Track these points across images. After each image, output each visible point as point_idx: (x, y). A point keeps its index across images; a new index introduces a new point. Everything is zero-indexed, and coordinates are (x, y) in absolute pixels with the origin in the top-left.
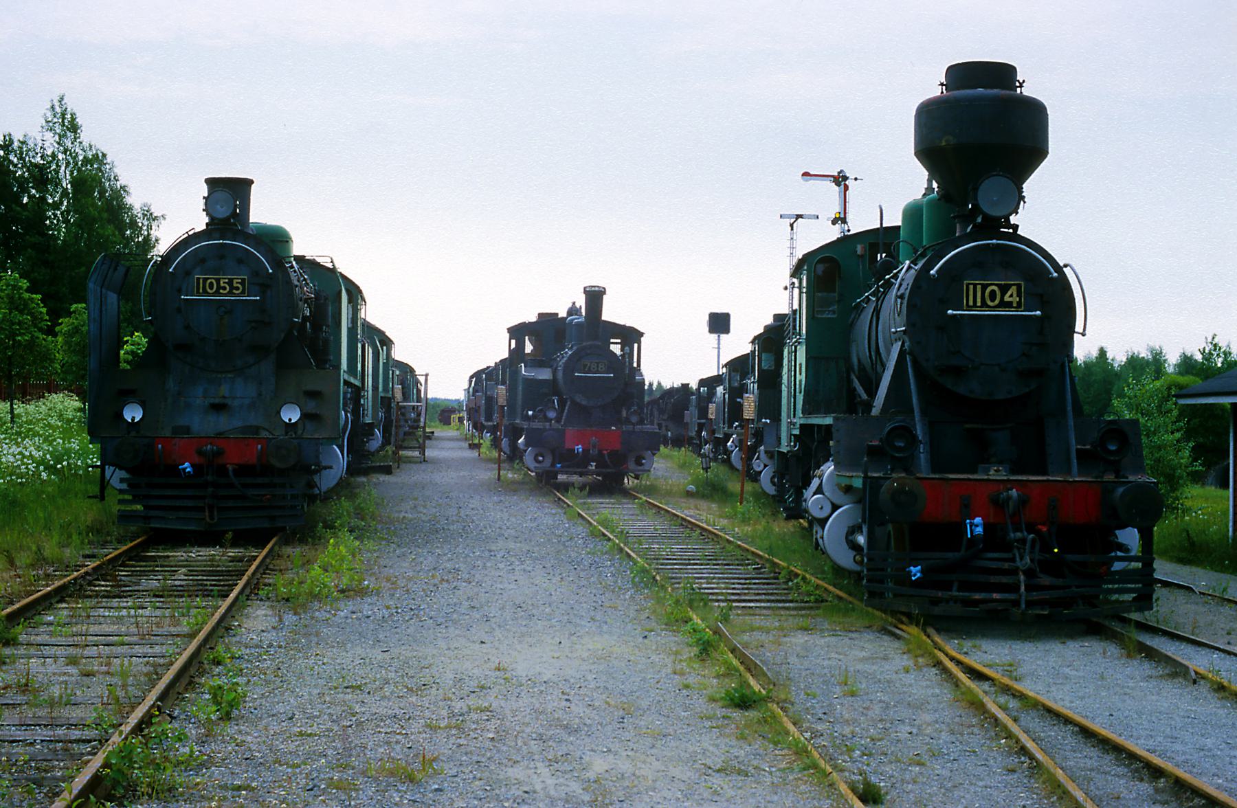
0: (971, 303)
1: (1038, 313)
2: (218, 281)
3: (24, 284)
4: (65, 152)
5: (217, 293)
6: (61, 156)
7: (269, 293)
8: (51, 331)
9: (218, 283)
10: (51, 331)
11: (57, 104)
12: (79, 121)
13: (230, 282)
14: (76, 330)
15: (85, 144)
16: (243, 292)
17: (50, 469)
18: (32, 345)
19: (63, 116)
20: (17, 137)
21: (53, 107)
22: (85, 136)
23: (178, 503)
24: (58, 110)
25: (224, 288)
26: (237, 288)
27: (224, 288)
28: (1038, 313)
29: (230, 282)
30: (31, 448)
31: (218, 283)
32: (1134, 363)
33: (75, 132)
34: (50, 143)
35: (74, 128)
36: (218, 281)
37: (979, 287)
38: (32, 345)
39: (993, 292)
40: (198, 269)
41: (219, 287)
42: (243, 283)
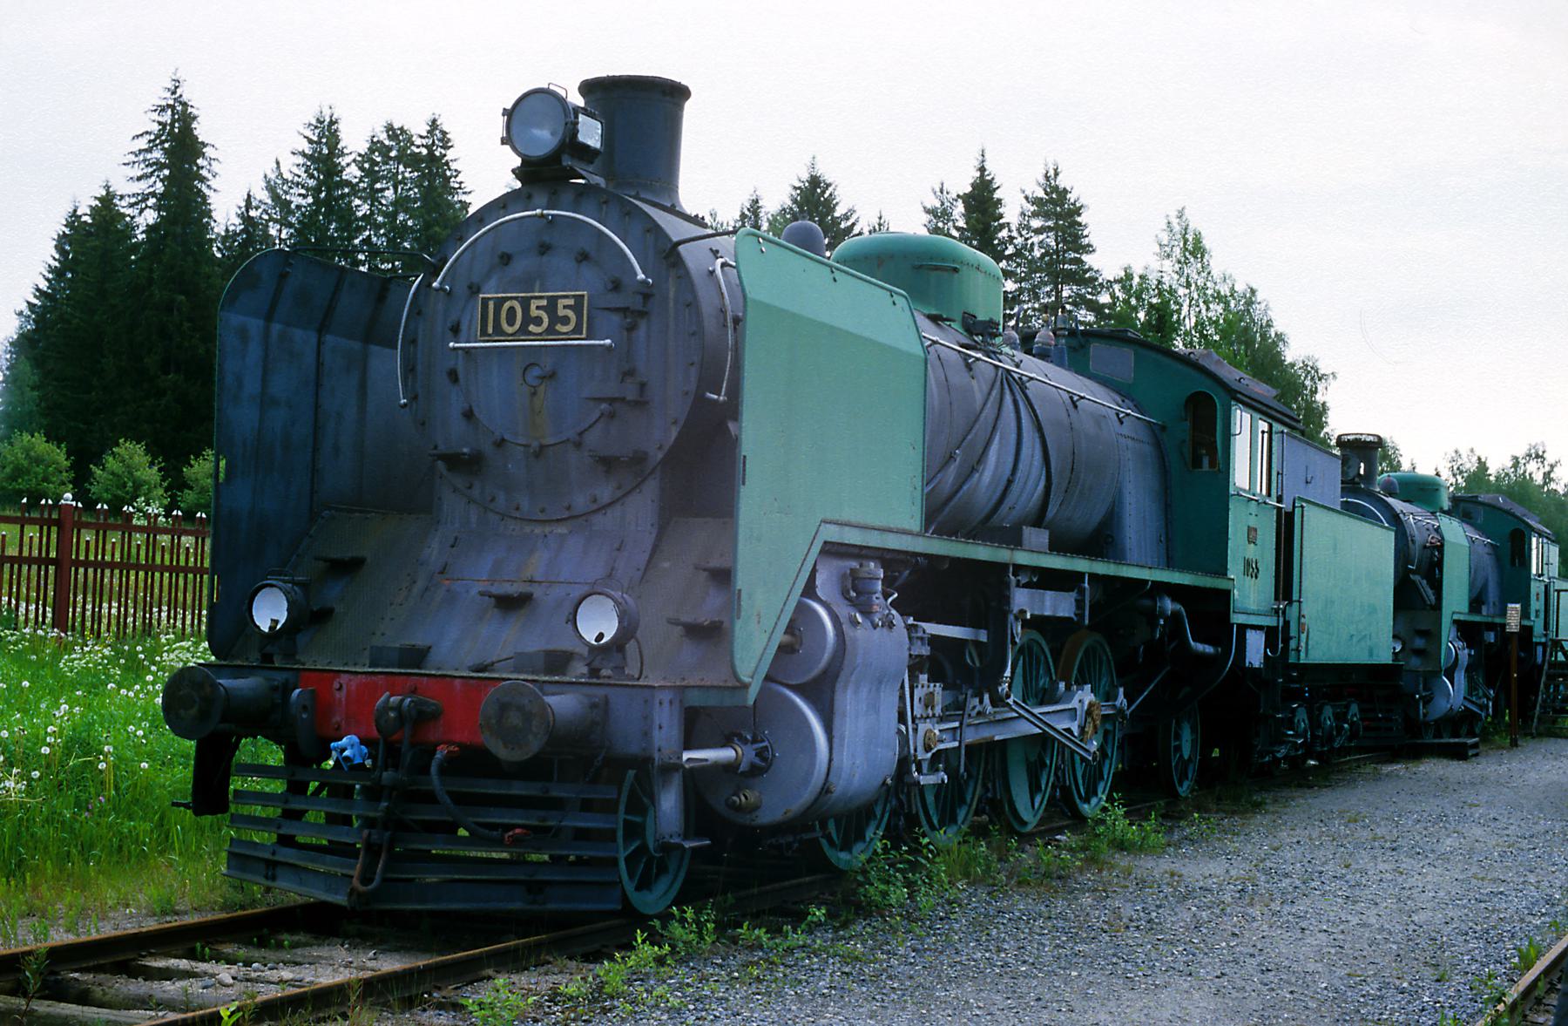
1: (608, 341)
2: (525, 303)
4: (1188, 285)
5: (523, 330)
6: (1182, 291)
7: (641, 332)
9: (526, 309)
11: (1175, 221)
12: (1206, 243)
13: (551, 307)
16: (577, 329)
20: (1137, 271)
22: (1217, 265)
24: (1177, 228)
25: (538, 321)
26: (565, 320)
27: (538, 321)
28: (608, 341)
29: (551, 307)
31: (526, 309)
32: (59, 248)
34: (1167, 271)
35: (1195, 249)
36: (525, 303)
37: (491, 305)
40: (493, 282)
41: (528, 319)
42: (577, 308)
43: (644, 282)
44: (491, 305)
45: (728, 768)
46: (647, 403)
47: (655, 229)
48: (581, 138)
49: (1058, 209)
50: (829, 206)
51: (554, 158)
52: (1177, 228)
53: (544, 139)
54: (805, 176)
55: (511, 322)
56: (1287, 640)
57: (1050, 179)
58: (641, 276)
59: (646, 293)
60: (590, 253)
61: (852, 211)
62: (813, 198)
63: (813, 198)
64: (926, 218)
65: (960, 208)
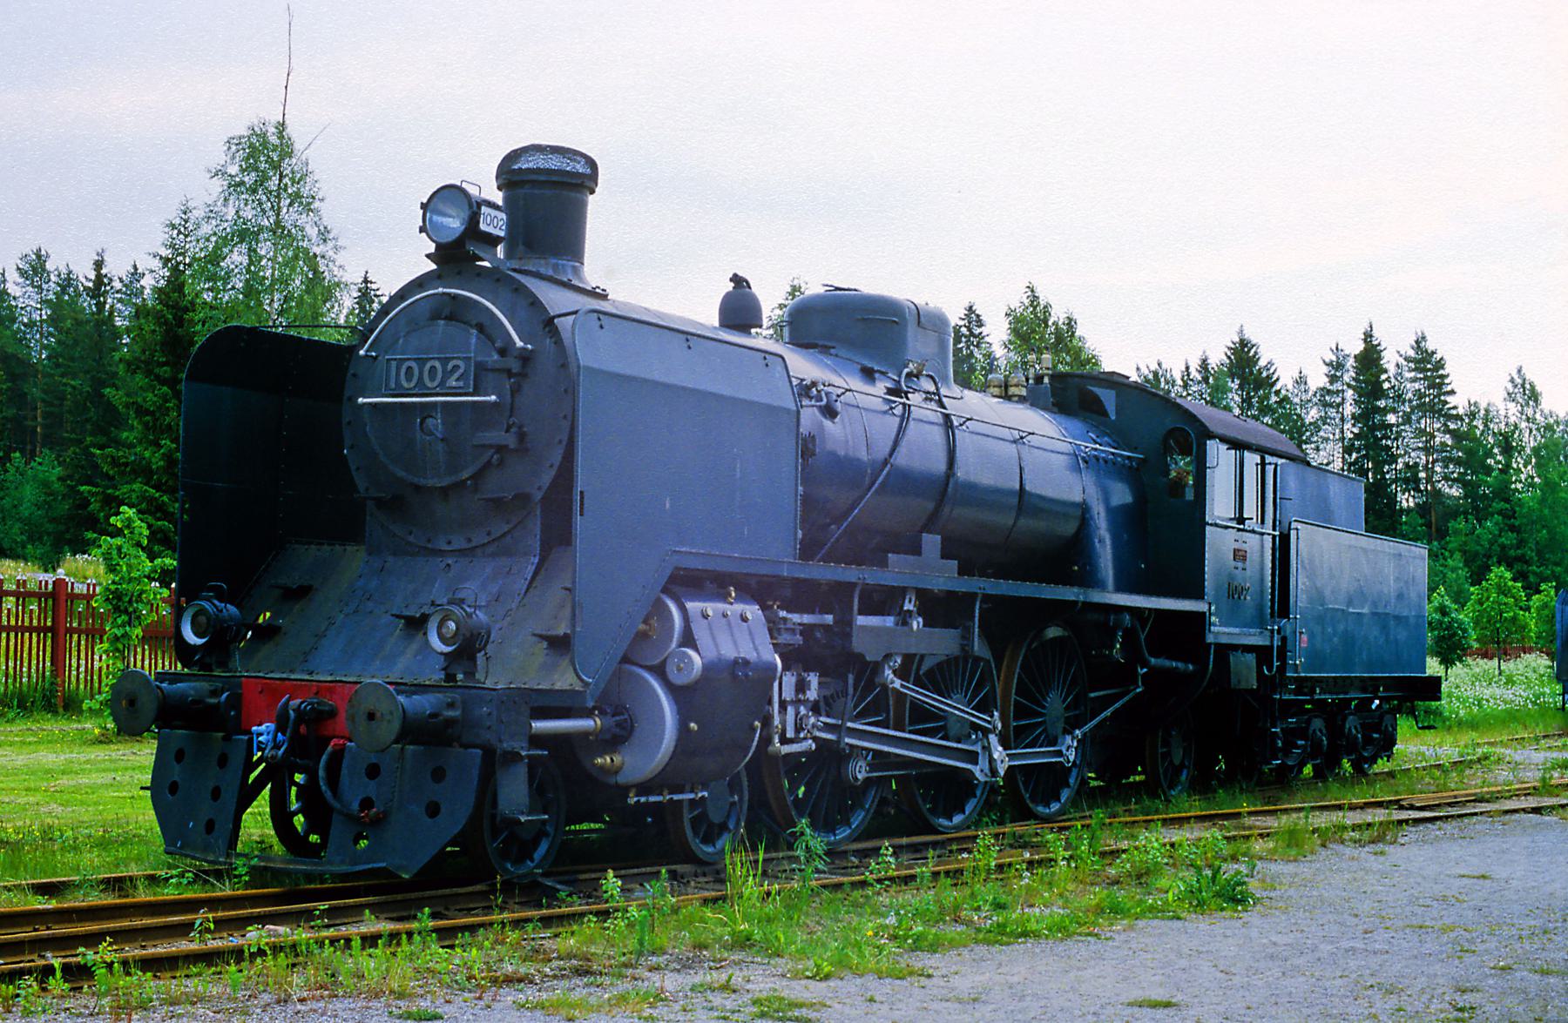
0: (12, 635)
1: (493, 398)
3: (1508, 575)
6: (1524, 425)
8: (1528, 609)
10: (1528, 609)
12: (1538, 389)
14: (1545, 606)
15: (1546, 412)
17: (1534, 703)
18: (1514, 619)
19: (1523, 386)
21: (1512, 380)
22: (1546, 404)
23: (34, 662)
24: (1519, 381)
28: (493, 398)
30: (1520, 690)
33: (1536, 401)
35: (1534, 396)
37: (394, 364)
38: (1514, 619)
39: (409, 368)
43: (524, 349)
44: (394, 364)
45: (584, 735)
46: (527, 450)
47: (535, 303)
48: (483, 227)
49: (1426, 362)
50: (1254, 361)
51: (459, 242)
52: (1519, 381)
53: (454, 224)
54: (1237, 339)
55: (432, 379)
56: (1282, 656)
57: (1419, 344)
58: (519, 344)
59: (525, 358)
60: (487, 328)
61: (1270, 363)
62: (1243, 358)
63: (1243, 358)
64: (1325, 369)
65: (1351, 362)
